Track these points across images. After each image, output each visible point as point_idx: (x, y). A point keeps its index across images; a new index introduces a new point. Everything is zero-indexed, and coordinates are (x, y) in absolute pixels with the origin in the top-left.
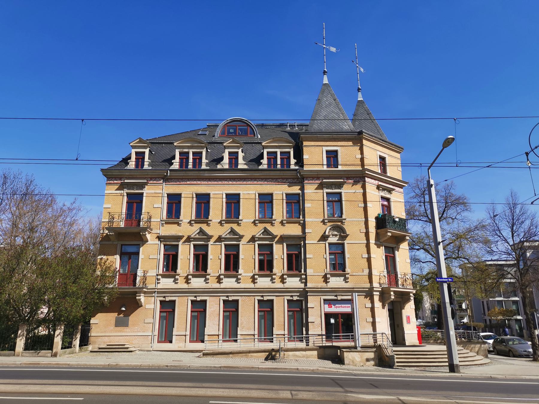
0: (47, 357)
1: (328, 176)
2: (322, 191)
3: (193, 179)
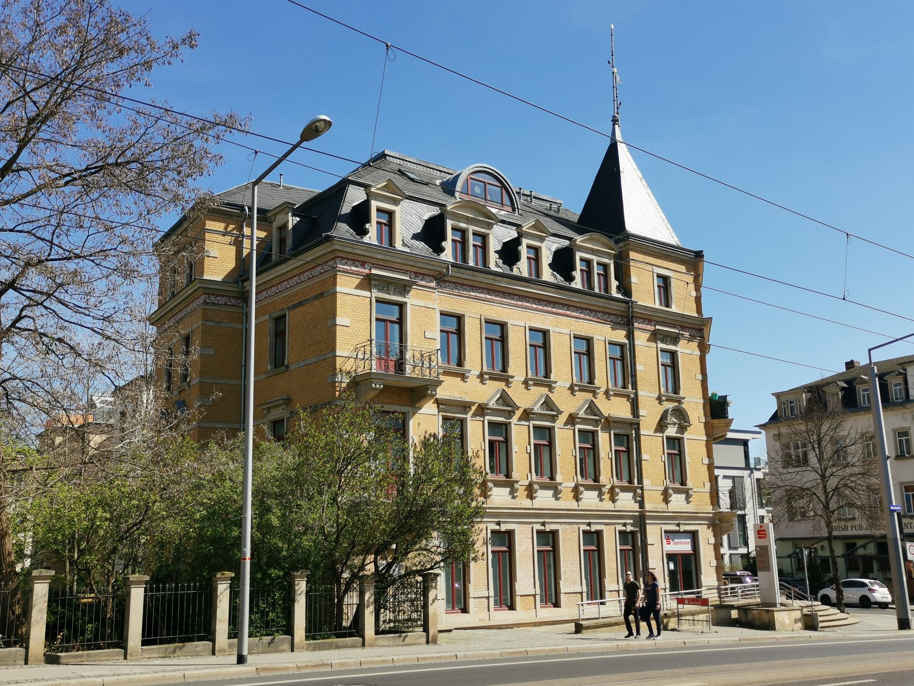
0: (419, 644)
1: (662, 320)
2: (368, 294)
3: (479, 288)
